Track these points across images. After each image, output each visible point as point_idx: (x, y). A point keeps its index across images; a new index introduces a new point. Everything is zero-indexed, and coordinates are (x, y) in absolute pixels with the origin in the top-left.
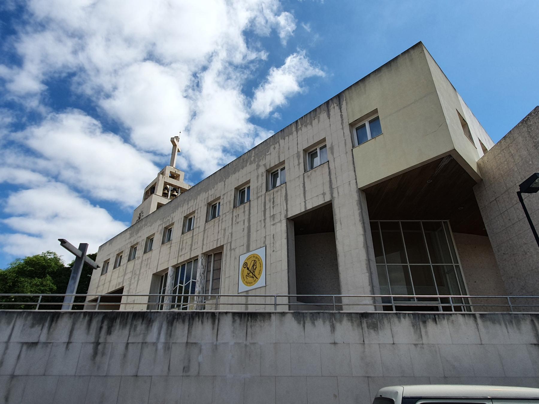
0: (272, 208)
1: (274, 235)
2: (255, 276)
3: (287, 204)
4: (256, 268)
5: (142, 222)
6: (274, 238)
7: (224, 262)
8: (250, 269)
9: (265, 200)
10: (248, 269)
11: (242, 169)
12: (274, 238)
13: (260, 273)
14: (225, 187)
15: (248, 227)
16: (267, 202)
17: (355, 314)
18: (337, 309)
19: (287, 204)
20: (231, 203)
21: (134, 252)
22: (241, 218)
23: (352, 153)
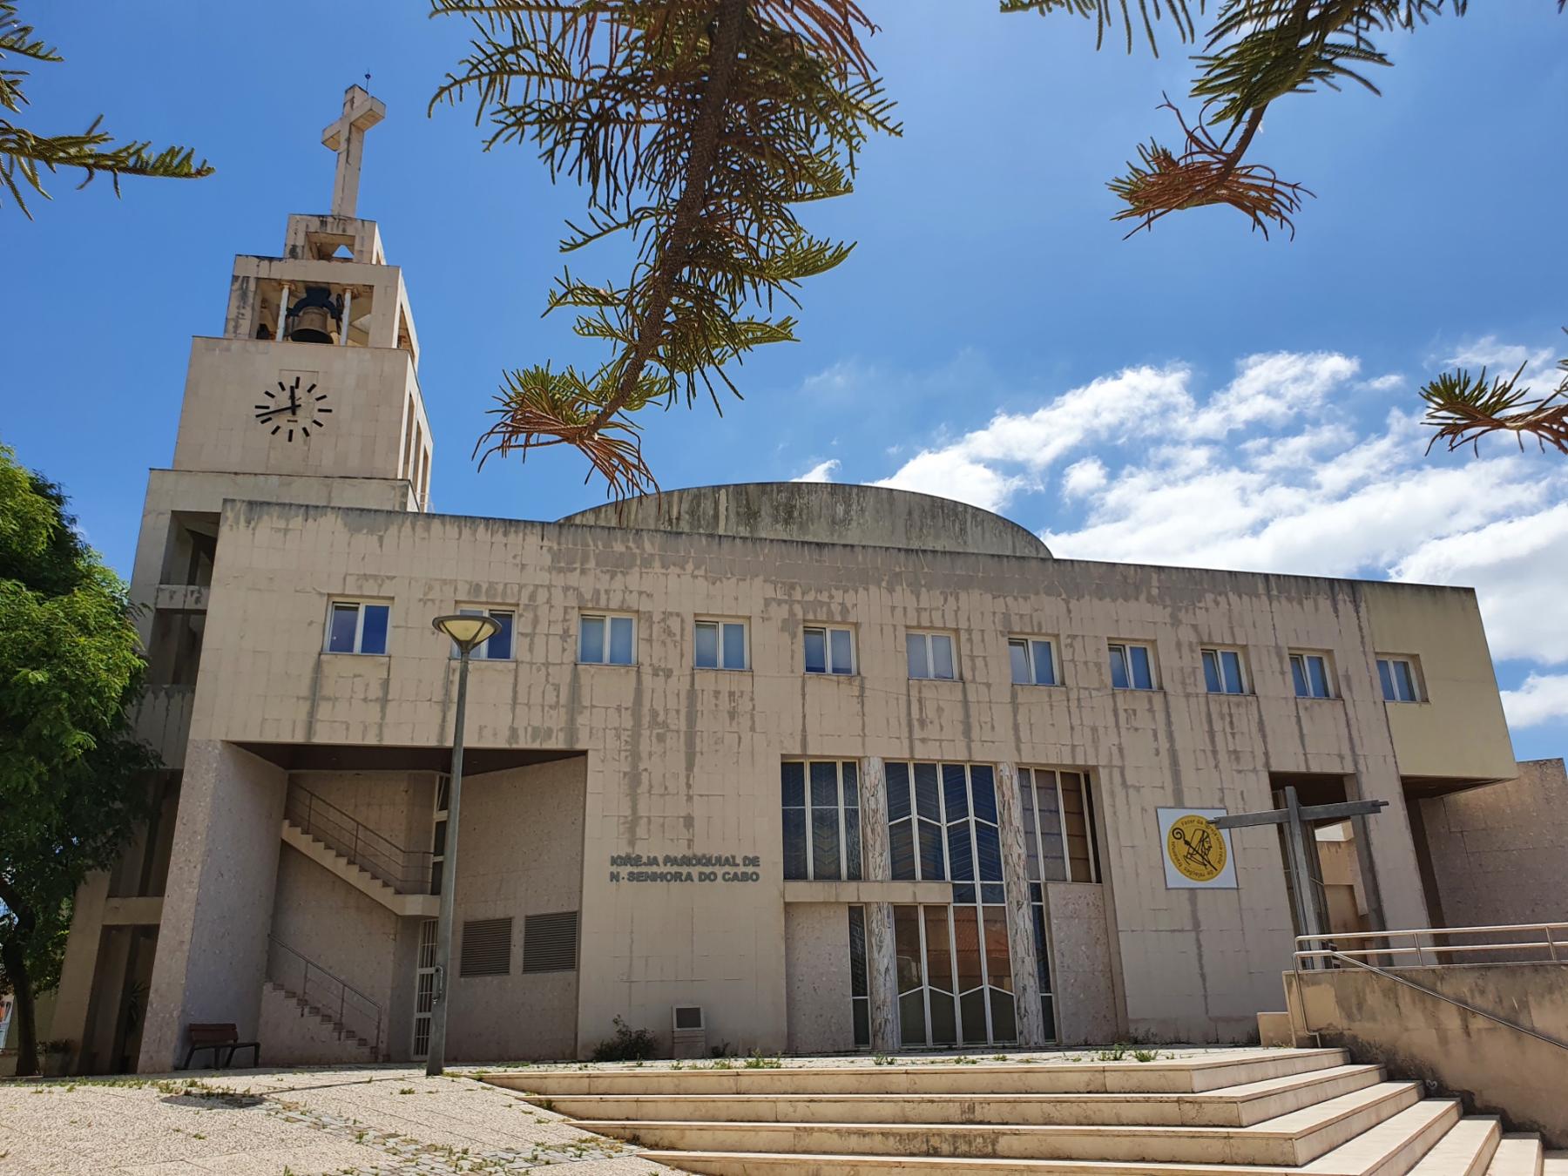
0: (1230, 737)
1: (1242, 793)
2: (1209, 862)
3: (1265, 743)
4: (1210, 847)
5: (1529, 1012)
6: (1243, 798)
7: (1105, 796)
8: (1193, 845)
9: (1209, 709)
10: (1187, 843)
11: (985, 467)
12: (1243, 798)
13: (1221, 860)
14: (1071, 619)
15: (1168, 750)
16: (1215, 716)
17: (234, 746)
18: (817, 813)
19: (1265, 743)
20: (1103, 671)
21: (406, 462)
22: (1143, 720)
23: (1125, 11)
